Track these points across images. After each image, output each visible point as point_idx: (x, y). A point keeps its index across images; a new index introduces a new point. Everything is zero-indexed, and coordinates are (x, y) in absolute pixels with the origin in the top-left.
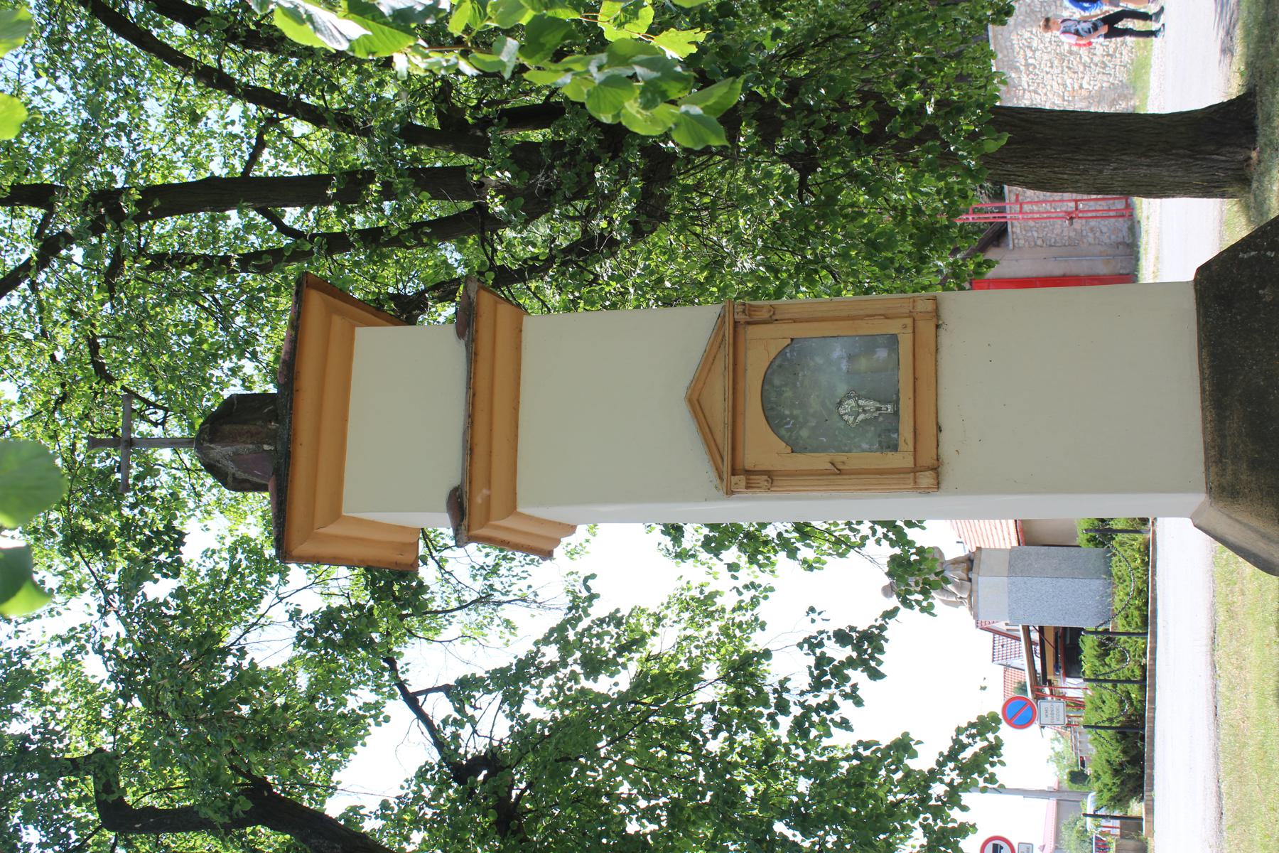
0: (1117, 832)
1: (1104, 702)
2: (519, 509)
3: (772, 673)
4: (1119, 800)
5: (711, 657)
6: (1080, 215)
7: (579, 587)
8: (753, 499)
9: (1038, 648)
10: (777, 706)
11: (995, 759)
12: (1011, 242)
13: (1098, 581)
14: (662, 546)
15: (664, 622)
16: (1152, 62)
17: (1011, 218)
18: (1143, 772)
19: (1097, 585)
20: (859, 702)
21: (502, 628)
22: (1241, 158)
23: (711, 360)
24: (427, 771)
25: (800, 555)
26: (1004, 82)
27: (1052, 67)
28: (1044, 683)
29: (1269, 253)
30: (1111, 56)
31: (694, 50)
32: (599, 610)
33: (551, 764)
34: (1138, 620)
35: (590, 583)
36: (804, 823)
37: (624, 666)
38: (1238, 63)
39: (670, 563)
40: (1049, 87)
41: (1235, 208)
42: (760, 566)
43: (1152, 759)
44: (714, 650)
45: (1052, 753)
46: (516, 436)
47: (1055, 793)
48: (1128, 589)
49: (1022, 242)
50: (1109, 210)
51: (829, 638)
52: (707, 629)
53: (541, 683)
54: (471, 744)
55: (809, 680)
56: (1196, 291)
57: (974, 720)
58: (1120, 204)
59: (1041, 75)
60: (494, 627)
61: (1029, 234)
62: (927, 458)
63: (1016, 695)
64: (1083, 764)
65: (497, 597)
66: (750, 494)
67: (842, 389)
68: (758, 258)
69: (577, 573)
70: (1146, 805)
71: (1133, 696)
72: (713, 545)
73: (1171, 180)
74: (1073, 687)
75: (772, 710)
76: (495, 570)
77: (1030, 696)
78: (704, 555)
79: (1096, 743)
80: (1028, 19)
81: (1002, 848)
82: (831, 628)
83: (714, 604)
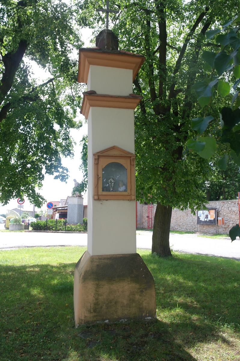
2: (91, 107)
43: (40, 232)
62: (101, 197)
77: (53, 207)
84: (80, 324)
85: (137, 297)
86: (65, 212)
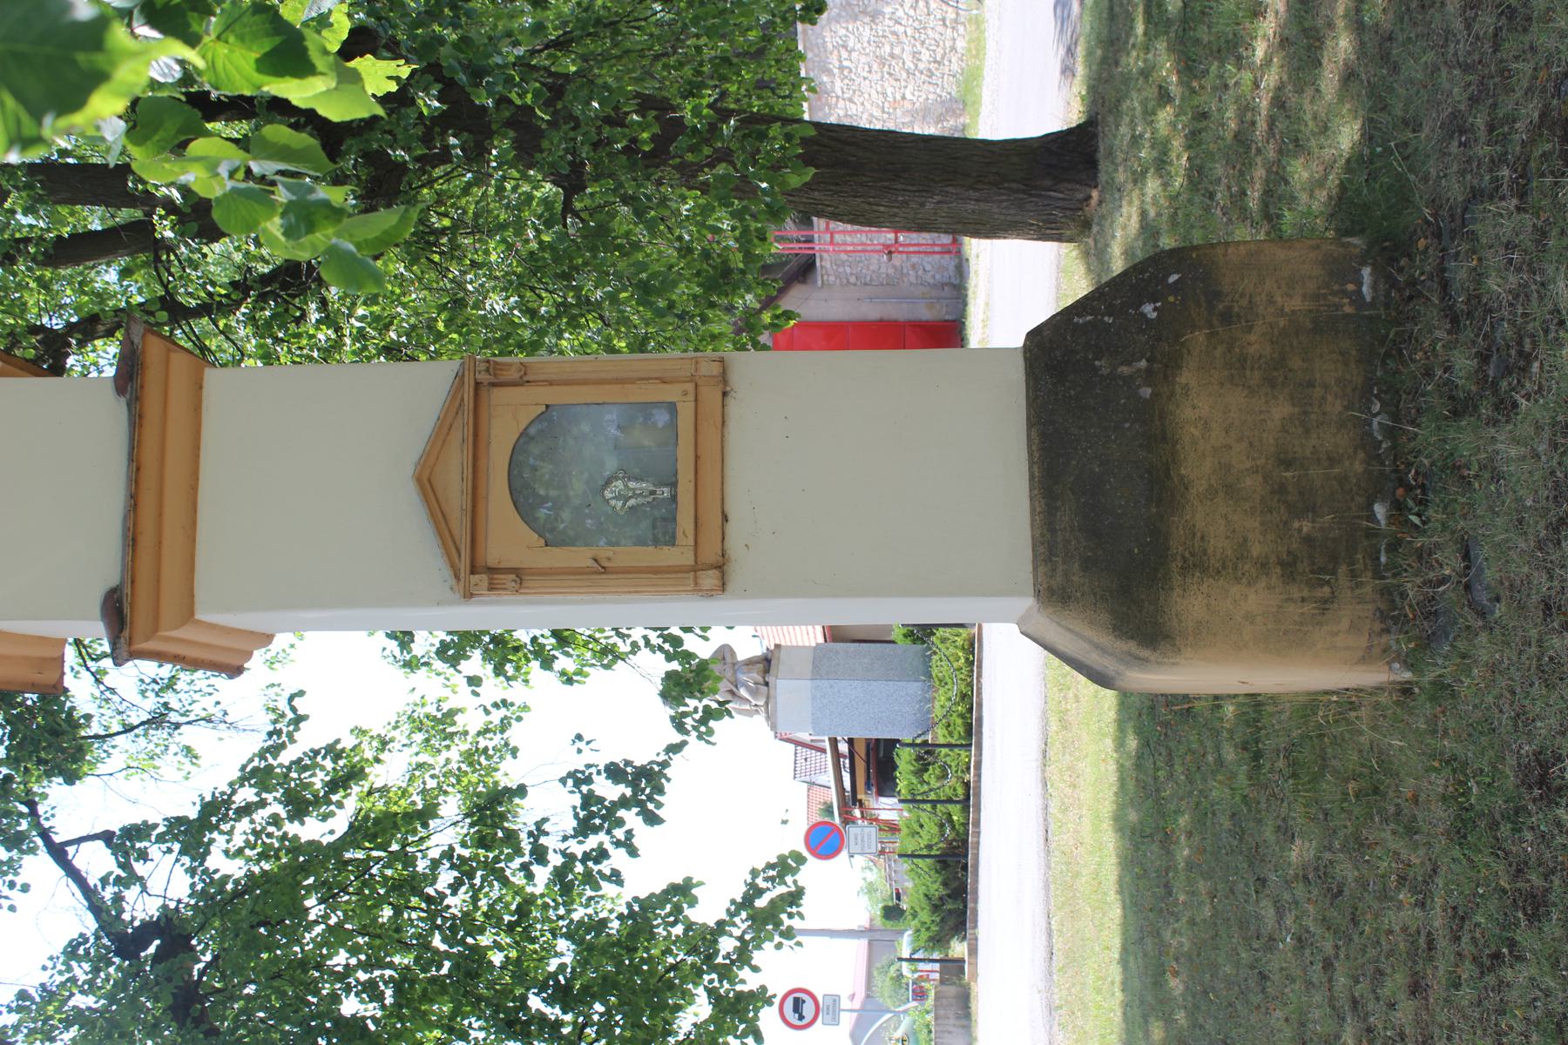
0: (937, 976)
1: (922, 826)
2: (198, 616)
3: (524, 816)
4: (939, 940)
5: (450, 789)
6: (901, 249)
7: (283, 705)
8: (497, 603)
9: (847, 761)
10: (532, 853)
11: (794, 910)
12: (819, 278)
13: (916, 684)
14: (387, 652)
15: (390, 746)
16: (985, 74)
17: (820, 250)
18: (966, 907)
19: (914, 688)
20: (633, 852)
21: (180, 757)
22: (1080, 196)
23: (446, 429)
24: (80, 944)
25: (558, 665)
26: (812, 90)
27: (870, 72)
28: (854, 804)
29: (1106, 319)
30: (939, 63)
31: (393, 87)
32: (309, 739)
33: (245, 933)
34: (961, 730)
35: (296, 702)
36: (563, 995)
37: (340, 805)
38: (1079, 87)
39: (399, 673)
40: (866, 96)
41: (1075, 253)
42: (508, 679)
44: (453, 780)
45: (862, 883)
46: (194, 523)
47: (867, 932)
48: (950, 694)
49: (832, 278)
50: (934, 245)
51: (599, 773)
52: (445, 754)
53: (233, 828)
54: (139, 906)
55: (575, 823)
56: (1026, 359)
57: (774, 860)
58: (946, 239)
59: (858, 81)
60: (169, 757)
61: (841, 270)
62: (710, 554)
63: (819, 819)
64: (898, 897)
65: (174, 717)
66: (494, 598)
67: (611, 464)
68: (512, 299)
69: (279, 685)
70: (969, 945)
71: (955, 818)
72: (450, 653)
73: (1002, 217)
74: (887, 808)
75: (526, 859)
76: (171, 684)
77: (837, 820)
78: (438, 665)
79: (913, 874)
80: (843, 14)
81: (804, 1002)
82: (602, 761)
83: (454, 724)
84: (1388, 656)
85: (1255, 343)
86: (868, 754)
